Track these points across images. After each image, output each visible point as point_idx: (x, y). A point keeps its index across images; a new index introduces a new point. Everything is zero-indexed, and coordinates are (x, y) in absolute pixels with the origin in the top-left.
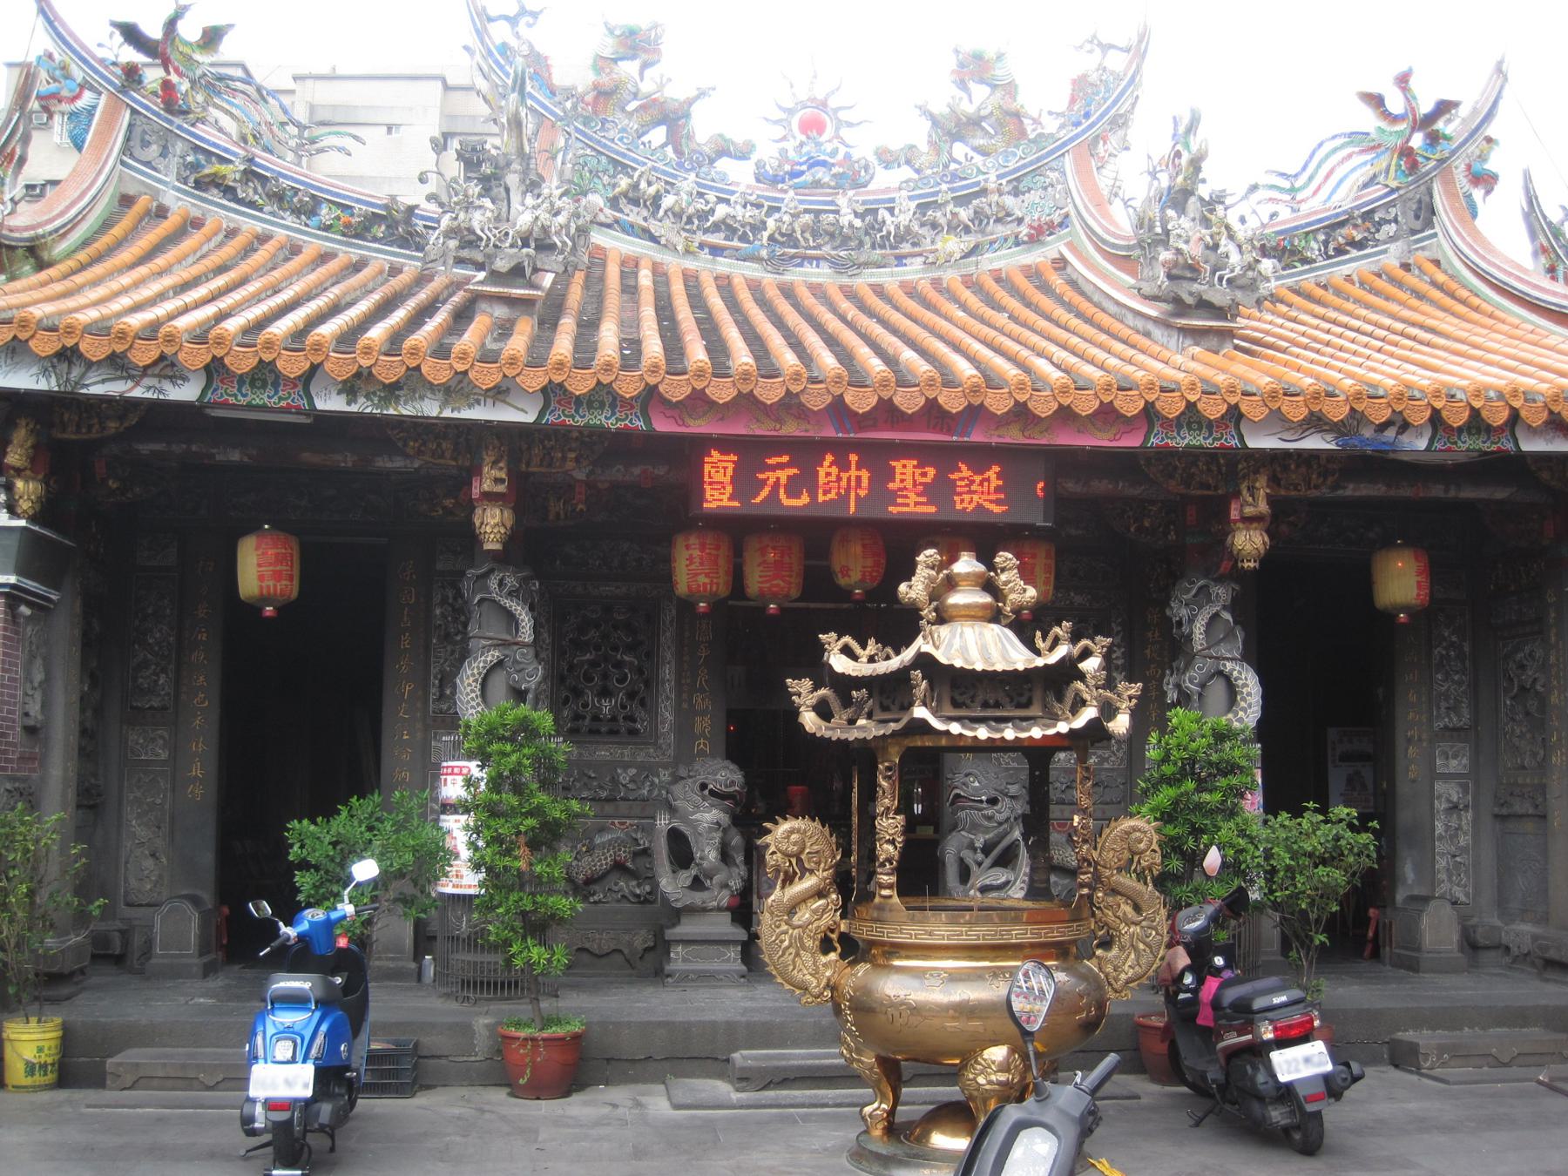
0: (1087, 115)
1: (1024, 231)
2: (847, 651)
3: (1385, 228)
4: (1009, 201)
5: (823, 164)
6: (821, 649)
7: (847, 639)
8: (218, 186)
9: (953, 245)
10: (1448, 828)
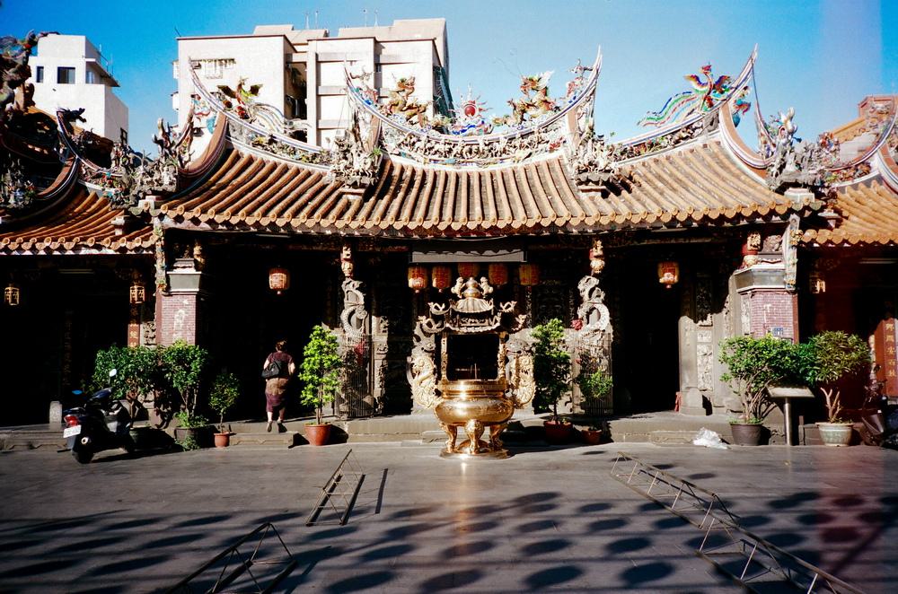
0: (575, 98)
1: (548, 146)
2: (436, 307)
3: (697, 131)
4: (543, 135)
5: (474, 126)
6: (429, 307)
7: (436, 304)
8: (261, 145)
9: (522, 153)
10: (702, 361)
